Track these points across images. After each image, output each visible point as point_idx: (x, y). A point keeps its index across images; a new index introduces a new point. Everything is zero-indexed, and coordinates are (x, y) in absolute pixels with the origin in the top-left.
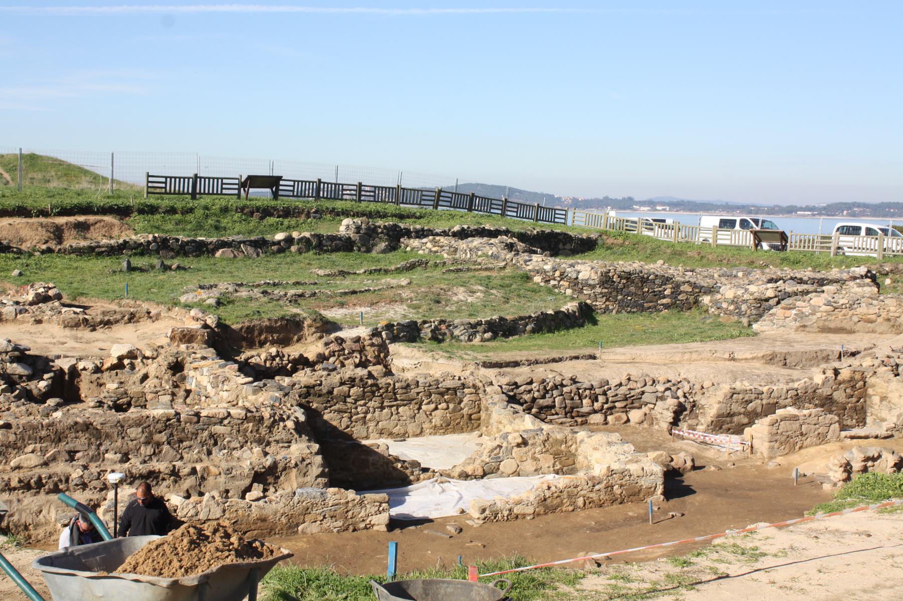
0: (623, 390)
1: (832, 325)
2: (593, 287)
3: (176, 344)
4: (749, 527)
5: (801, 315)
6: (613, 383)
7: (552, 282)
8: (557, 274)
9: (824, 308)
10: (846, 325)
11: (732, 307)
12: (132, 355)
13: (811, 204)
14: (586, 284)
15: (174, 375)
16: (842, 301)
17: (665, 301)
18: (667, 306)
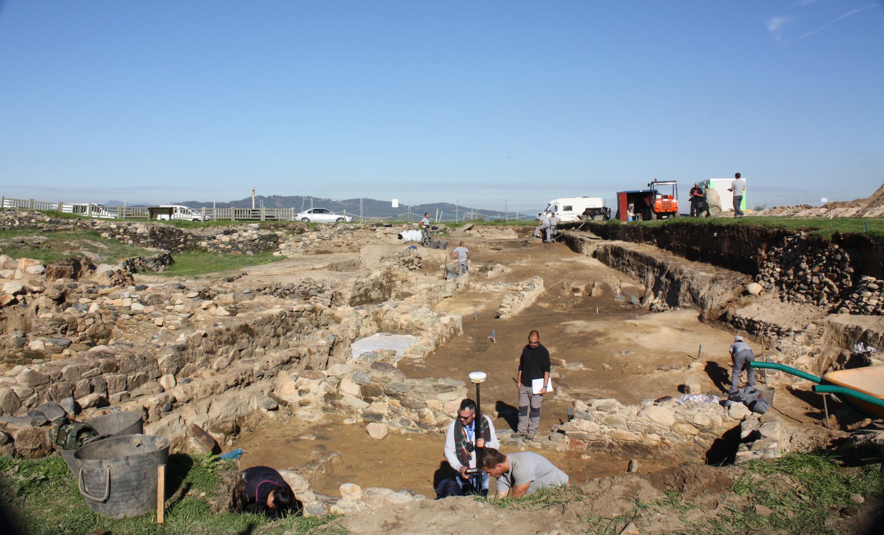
0: (302, 289)
1: (322, 250)
2: (146, 238)
3: (52, 279)
4: (539, 287)
5: (305, 245)
6: (297, 284)
7: (118, 236)
8: (121, 230)
9: (317, 240)
10: (328, 249)
11: (230, 247)
12: (23, 292)
13: (201, 198)
14: (142, 236)
15: (58, 305)
16: (326, 236)
17: (181, 246)
18: (182, 249)
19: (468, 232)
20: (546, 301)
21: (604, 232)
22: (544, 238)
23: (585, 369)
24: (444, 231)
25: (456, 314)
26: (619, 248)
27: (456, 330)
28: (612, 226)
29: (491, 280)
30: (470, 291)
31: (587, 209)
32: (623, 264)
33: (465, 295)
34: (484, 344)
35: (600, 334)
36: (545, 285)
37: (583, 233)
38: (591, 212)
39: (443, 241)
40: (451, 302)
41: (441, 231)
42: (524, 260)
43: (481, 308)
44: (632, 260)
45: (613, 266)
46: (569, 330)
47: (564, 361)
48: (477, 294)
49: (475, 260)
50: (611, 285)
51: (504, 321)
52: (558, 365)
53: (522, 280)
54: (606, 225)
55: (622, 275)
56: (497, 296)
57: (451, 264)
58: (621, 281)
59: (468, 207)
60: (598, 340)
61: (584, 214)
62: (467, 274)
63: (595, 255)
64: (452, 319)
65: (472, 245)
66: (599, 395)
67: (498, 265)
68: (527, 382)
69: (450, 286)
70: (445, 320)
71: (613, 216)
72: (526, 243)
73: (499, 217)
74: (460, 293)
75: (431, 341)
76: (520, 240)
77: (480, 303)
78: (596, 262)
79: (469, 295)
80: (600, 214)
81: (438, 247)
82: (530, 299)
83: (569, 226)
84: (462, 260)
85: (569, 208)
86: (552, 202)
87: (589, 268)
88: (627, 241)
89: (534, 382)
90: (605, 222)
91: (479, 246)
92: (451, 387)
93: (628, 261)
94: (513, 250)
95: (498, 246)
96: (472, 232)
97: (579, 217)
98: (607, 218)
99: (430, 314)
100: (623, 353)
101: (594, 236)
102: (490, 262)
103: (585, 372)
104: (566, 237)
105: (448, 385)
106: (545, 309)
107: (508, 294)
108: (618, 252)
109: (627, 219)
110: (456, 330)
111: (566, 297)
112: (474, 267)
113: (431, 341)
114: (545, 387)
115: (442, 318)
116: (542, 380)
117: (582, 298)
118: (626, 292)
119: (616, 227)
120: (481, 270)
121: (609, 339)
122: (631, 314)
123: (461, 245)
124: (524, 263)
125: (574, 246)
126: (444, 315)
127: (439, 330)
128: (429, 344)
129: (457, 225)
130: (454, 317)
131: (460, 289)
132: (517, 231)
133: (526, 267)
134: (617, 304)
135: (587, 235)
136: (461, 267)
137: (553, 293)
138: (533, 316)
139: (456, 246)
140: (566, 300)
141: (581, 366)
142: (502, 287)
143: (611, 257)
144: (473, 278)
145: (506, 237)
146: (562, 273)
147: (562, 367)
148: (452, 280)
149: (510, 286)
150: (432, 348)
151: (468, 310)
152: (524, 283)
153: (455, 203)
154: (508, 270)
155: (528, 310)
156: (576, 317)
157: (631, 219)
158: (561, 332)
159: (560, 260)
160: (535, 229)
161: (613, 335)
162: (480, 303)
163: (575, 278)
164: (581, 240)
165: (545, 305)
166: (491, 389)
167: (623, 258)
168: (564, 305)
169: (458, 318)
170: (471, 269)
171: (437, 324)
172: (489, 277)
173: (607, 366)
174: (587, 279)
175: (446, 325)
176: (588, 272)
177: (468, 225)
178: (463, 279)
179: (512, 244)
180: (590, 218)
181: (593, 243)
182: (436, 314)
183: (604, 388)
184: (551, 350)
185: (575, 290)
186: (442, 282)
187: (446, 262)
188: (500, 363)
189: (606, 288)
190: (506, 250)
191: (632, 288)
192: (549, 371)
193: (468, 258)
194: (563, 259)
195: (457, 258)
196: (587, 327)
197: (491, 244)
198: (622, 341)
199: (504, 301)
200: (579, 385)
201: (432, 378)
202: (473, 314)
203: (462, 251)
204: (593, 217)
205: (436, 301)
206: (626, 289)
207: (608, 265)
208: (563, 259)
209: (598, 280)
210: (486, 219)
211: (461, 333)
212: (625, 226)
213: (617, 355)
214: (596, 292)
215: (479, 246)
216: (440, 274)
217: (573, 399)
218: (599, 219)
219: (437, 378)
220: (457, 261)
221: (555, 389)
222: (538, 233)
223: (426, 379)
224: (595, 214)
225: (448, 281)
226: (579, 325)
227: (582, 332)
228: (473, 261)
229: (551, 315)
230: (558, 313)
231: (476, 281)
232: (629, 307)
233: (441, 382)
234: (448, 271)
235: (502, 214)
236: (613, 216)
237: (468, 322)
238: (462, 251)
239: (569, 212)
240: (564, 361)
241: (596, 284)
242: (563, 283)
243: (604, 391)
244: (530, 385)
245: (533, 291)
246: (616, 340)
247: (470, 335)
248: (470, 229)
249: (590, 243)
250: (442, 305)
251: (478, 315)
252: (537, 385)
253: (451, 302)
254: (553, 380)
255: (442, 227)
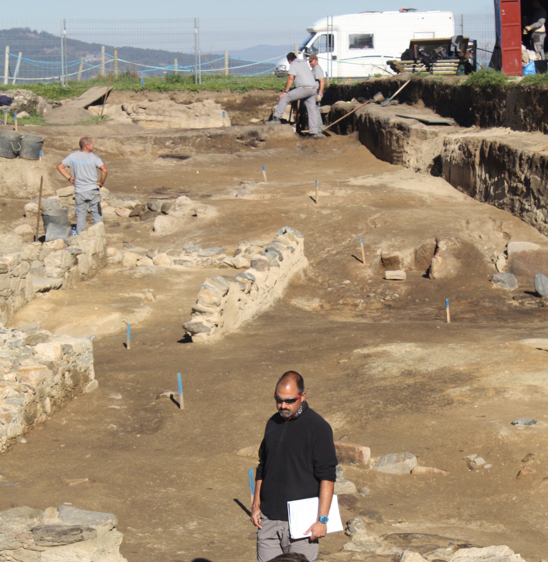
4: (293, 258)
19: (95, 110)
20: (314, 295)
21: (462, 105)
22: (302, 121)
23: (422, 469)
24: (30, 108)
25: (75, 336)
26: (502, 148)
27: (79, 379)
28: (484, 88)
29: (163, 241)
30: (110, 271)
31: (413, 43)
32: (514, 191)
33: (95, 281)
34: (155, 410)
35: (458, 379)
36: (308, 252)
37: (404, 109)
38: (424, 51)
39: (30, 134)
40: (59, 304)
41: (23, 108)
42: (250, 187)
43: (142, 315)
44: (535, 179)
45: (487, 198)
46: (376, 368)
47: (366, 451)
48: (128, 280)
49: (119, 188)
50: (483, 247)
51: (205, 350)
52: (352, 460)
53: (246, 239)
54: (466, 88)
55: (510, 221)
56: (181, 283)
57: (54, 201)
58: (508, 236)
59: (89, 40)
60: (455, 392)
61: (406, 56)
62: (99, 226)
63: (438, 167)
64: (66, 350)
65: (109, 146)
66: (462, 537)
67: (183, 199)
68: (276, 510)
69: (55, 258)
70: (48, 351)
71: (483, 60)
72: (253, 139)
73: (176, 68)
74: (83, 278)
75: (14, 410)
76: (238, 131)
77: (137, 302)
78: (440, 188)
79: (106, 283)
80: (450, 55)
81: (17, 155)
82: (270, 289)
83: (366, 90)
84: (86, 188)
85: (365, 42)
86: (320, 26)
87: (422, 203)
88: (523, 128)
89: (296, 507)
90: (463, 79)
91: (127, 148)
92: (78, 529)
93: (527, 182)
94: (220, 157)
95: (180, 149)
96: (106, 109)
97: (392, 65)
98: (469, 68)
99: (7, 336)
100: (521, 426)
101: (434, 117)
102: (159, 192)
103: (422, 477)
104: (354, 118)
105: (69, 524)
106: (310, 315)
107: (213, 277)
108: (498, 160)
109: (521, 70)
110: (79, 379)
111: (363, 281)
112: (116, 207)
113: (14, 410)
114: (322, 520)
115: (40, 348)
116: (316, 500)
117: (408, 282)
118: (521, 265)
119: (493, 92)
120: (136, 214)
121: (482, 390)
122: (537, 323)
123: (82, 146)
124: (251, 193)
125: (381, 143)
126: (44, 339)
127: (34, 378)
128: (8, 418)
129: (64, 93)
130: (72, 342)
131: (82, 268)
132: (229, 107)
133: (256, 204)
134: (498, 297)
135: (417, 113)
136: (83, 209)
137: (329, 273)
138: (281, 335)
139: (65, 149)
140: (365, 290)
141: (412, 462)
142: (194, 258)
143: (480, 172)
144: (115, 236)
145: (198, 124)
146: (353, 218)
147: (362, 466)
148: (59, 242)
149: (214, 255)
150: (17, 427)
151: (109, 322)
152: (252, 248)
153: (55, 30)
154: (209, 213)
155: (266, 318)
156: (393, 335)
157: (531, 68)
158: (355, 375)
159: (349, 179)
160: (276, 100)
161: (492, 379)
162: (137, 302)
163: (387, 231)
164: (400, 127)
165: (311, 304)
166: (180, 530)
167: (512, 174)
168: (360, 302)
169: (82, 344)
170: (108, 211)
171: (28, 363)
172: (159, 232)
173: (480, 461)
174: (419, 231)
175: (51, 366)
176: (421, 213)
177: (96, 93)
178: (90, 239)
179: (215, 141)
180: (421, 68)
181: (433, 137)
182: (22, 336)
183: (472, 518)
184: (336, 422)
185: (388, 263)
186: (32, 249)
187: (40, 194)
188: (199, 460)
189: (468, 255)
190: (202, 158)
191: (538, 254)
192: (332, 478)
193: (102, 183)
194: (353, 181)
195: (72, 182)
196: (422, 360)
197: (159, 142)
198: (515, 394)
199: (203, 295)
200: (409, 512)
201: (25, 510)
202: (123, 333)
203: (85, 163)
204: (429, 63)
205: (18, 301)
206: (523, 256)
207: (473, 194)
208: (353, 181)
209: (447, 235)
210: (142, 75)
211: (93, 384)
212: (518, 87)
213: (504, 432)
214: (443, 266)
215: (127, 148)
216: (25, 227)
217: (395, 550)
218: (445, 71)
219: (38, 507)
220: (70, 189)
221: (347, 524)
222: (284, 110)
223: (11, 511)
224: (436, 57)
225: (48, 245)
226: (399, 357)
227: (409, 374)
228: (114, 189)
229: (326, 331)
230: (345, 326)
231: (125, 244)
232: (530, 303)
233: (51, 518)
234: (46, 219)
235: (184, 59)
236: (483, 60)
237: (109, 355)
238: (85, 163)
239: (366, 51)
240: (366, 451)
241: (442, 246)
242: (355, 245)
243: (474, 526)
244: (284, 516)
245: (279, 268)
246: (499, 392)
247: (117, 388)
248: (100, 102)
249: (424, 136)
250: (35, 312)
251: (134, 334)
252: (302, 514)
253: (59, 304)
254: (344, 500)
255: (22, 97)
